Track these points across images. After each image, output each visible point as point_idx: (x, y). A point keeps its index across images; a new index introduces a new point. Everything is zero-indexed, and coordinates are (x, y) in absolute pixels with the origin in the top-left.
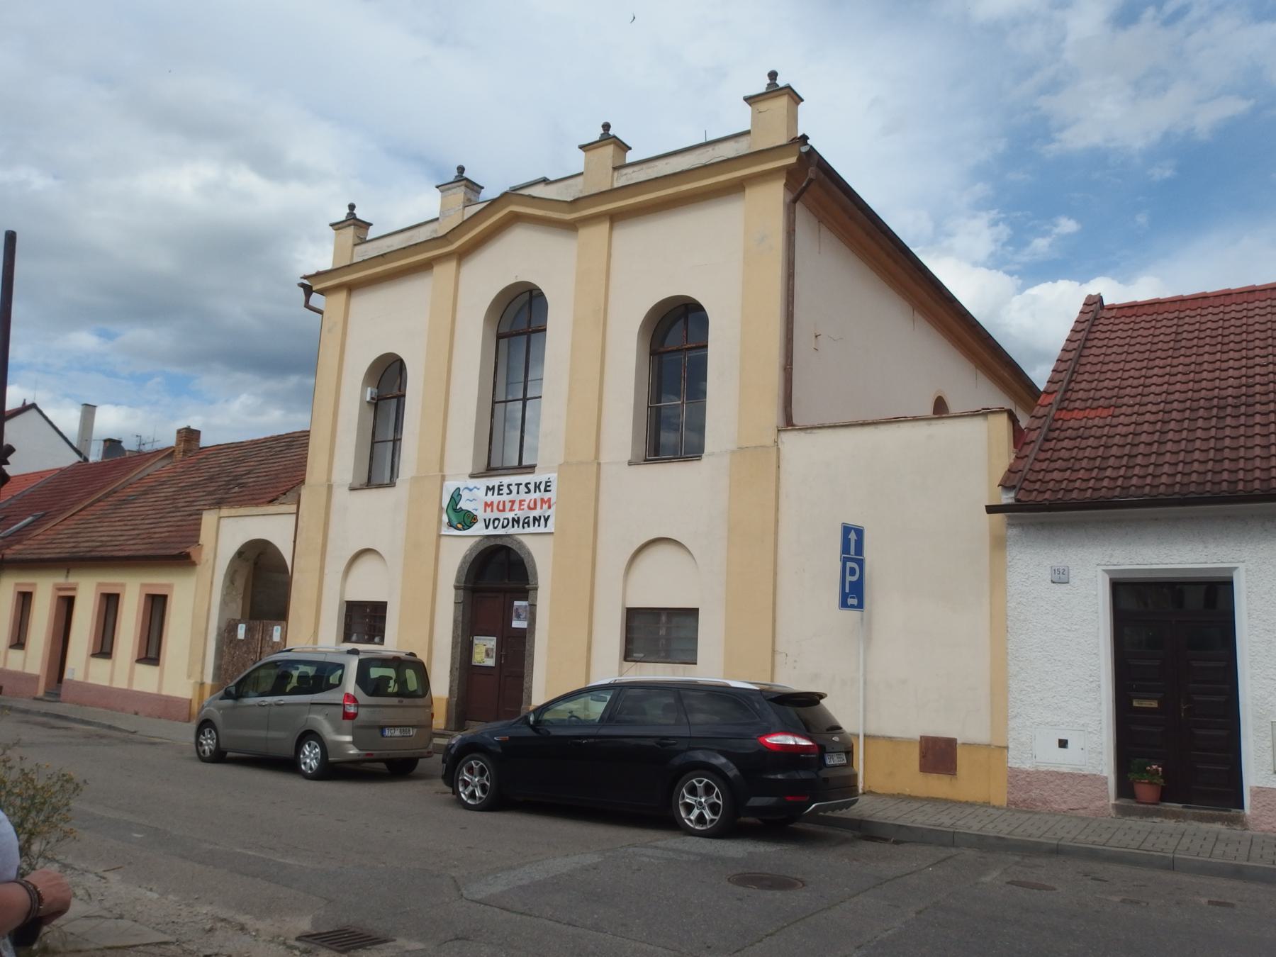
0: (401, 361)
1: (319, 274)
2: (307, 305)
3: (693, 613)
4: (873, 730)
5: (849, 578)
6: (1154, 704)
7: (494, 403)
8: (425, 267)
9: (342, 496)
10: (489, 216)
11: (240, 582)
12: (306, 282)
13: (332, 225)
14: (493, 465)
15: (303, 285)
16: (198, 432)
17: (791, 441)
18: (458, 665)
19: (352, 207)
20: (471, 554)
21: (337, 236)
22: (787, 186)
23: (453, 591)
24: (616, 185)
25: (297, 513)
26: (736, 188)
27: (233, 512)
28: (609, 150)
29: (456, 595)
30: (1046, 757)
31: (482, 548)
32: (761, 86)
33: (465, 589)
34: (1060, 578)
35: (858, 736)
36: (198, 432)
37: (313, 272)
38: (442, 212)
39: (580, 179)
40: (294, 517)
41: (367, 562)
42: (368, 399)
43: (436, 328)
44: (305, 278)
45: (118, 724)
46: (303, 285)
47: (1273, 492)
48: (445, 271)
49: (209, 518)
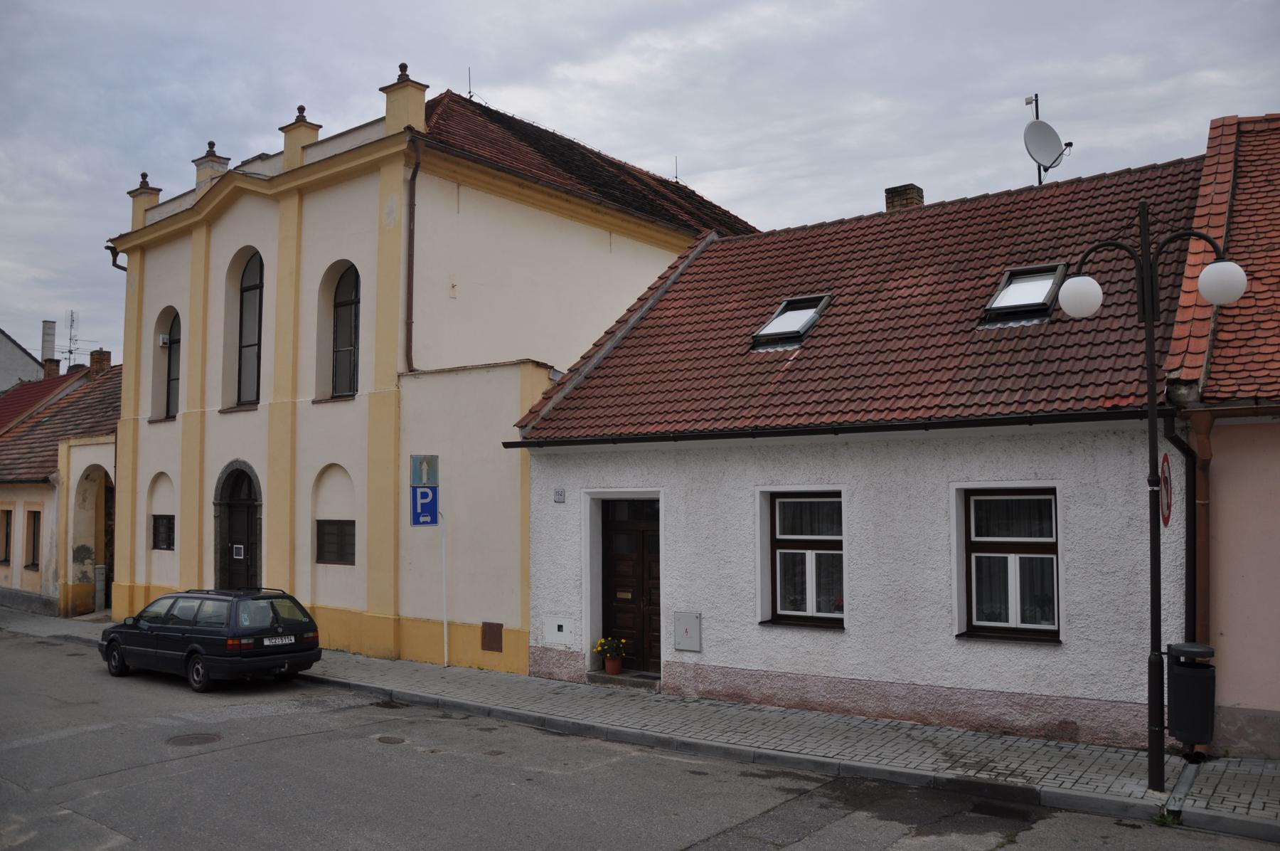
1: (121, 237)
2: (115, 264)
3: (352, 523)
4: (458, 620)
6: (629, 596)
8: (186, 232)
9: (144, 426)
10: (226, 186)
11: (91, 500)
12: (110, 244)
14: (244, 399)
15: (107, 248)
16: (109, 353)
17: (409, 384)
19: (144, 176)
23: (212, 507)
26: (373, 168)
30: (553, 639)
32: (393, 78)
33: (220, 505)
34: (560, 498)
36: (109, 353)
38: (197, 184)
41: (333, 480)
43: (194, 281)
44: (111, 240)
45: (31, 633)
46: (107, 248)
47: (1269, 391)
48: (199, 235)
49: (62, 448)
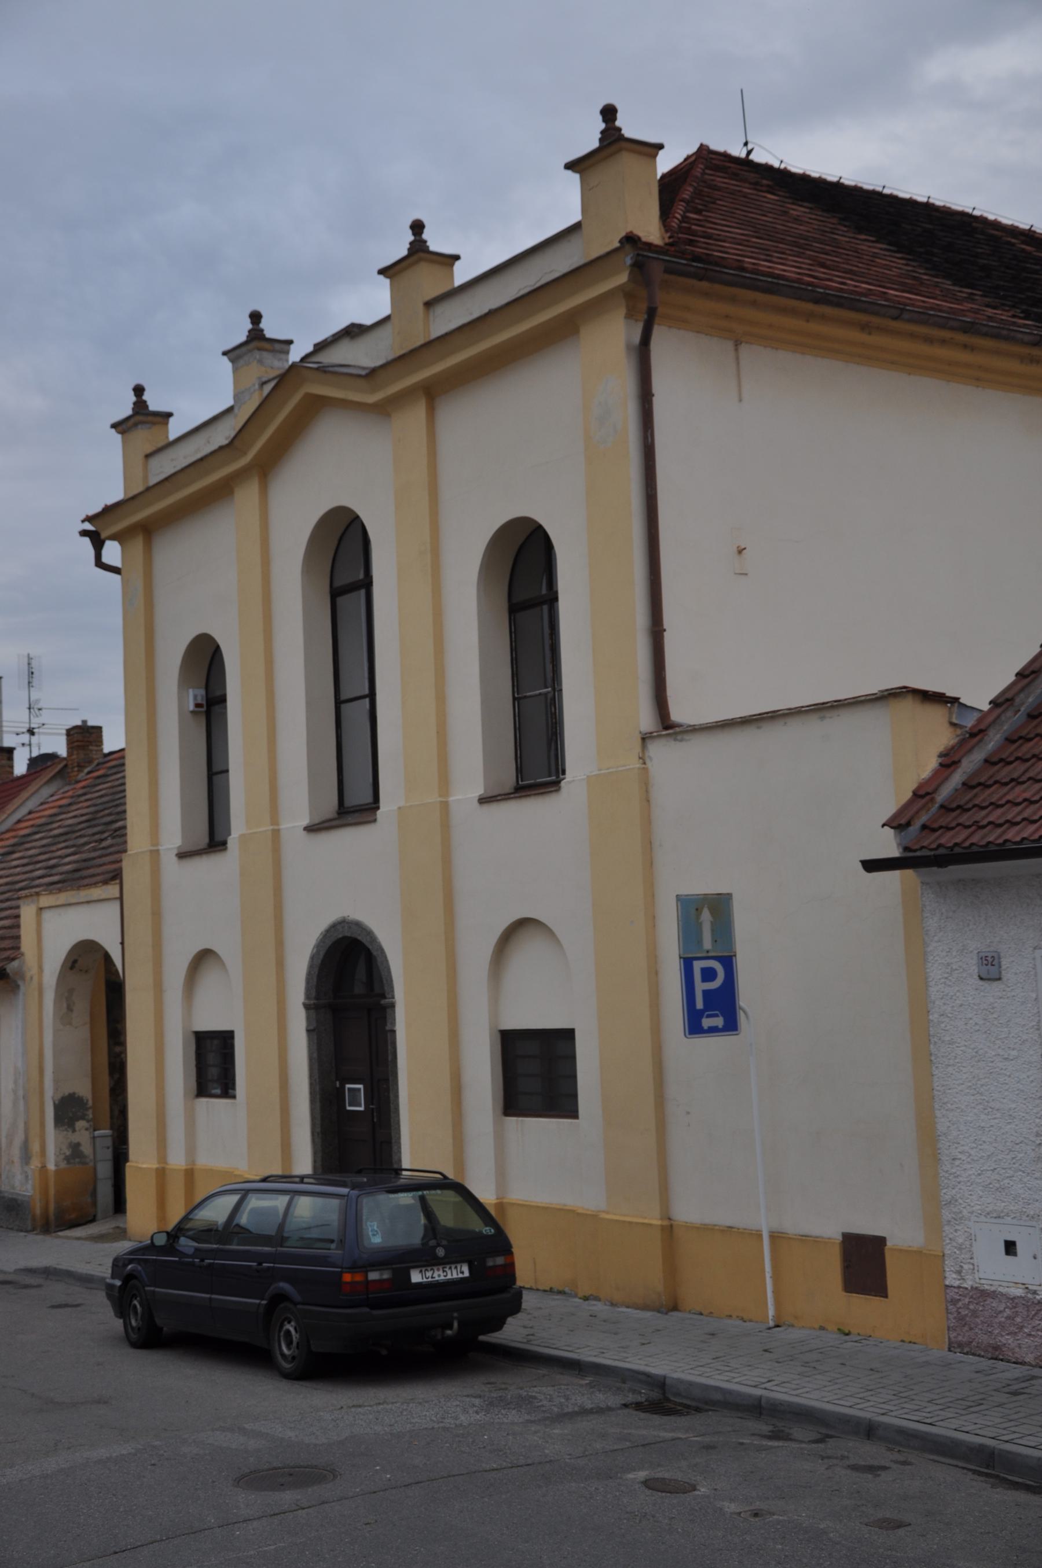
0: (218, 649)
1: (108, 510)
2: (99, 563)
5: (700, 986)
7: (339, 703)
8: (221, 492)
10: (291, 393)
11: (82, 1007)
12: (88, 526)
13: (114, 426)
15: (84, 533)
18: (318, 1130)
20: (318, 952)
21: (124, 442)
22: (630, 315)
24: (153, 480)
25: (121, 898)
26: (564, 330)
27: (63, 898)
28: (628, 161)
29: (308, 1018)
31: (329, 943)
34: (990, 969)
35: (759, 1236)
37: (97, 508)
39: (388, 329)
40: (117, 904)
42: (191, 707)
44: (89, 519)
46: (84, 533)
48: (247, 495)
49: (27, 912)
